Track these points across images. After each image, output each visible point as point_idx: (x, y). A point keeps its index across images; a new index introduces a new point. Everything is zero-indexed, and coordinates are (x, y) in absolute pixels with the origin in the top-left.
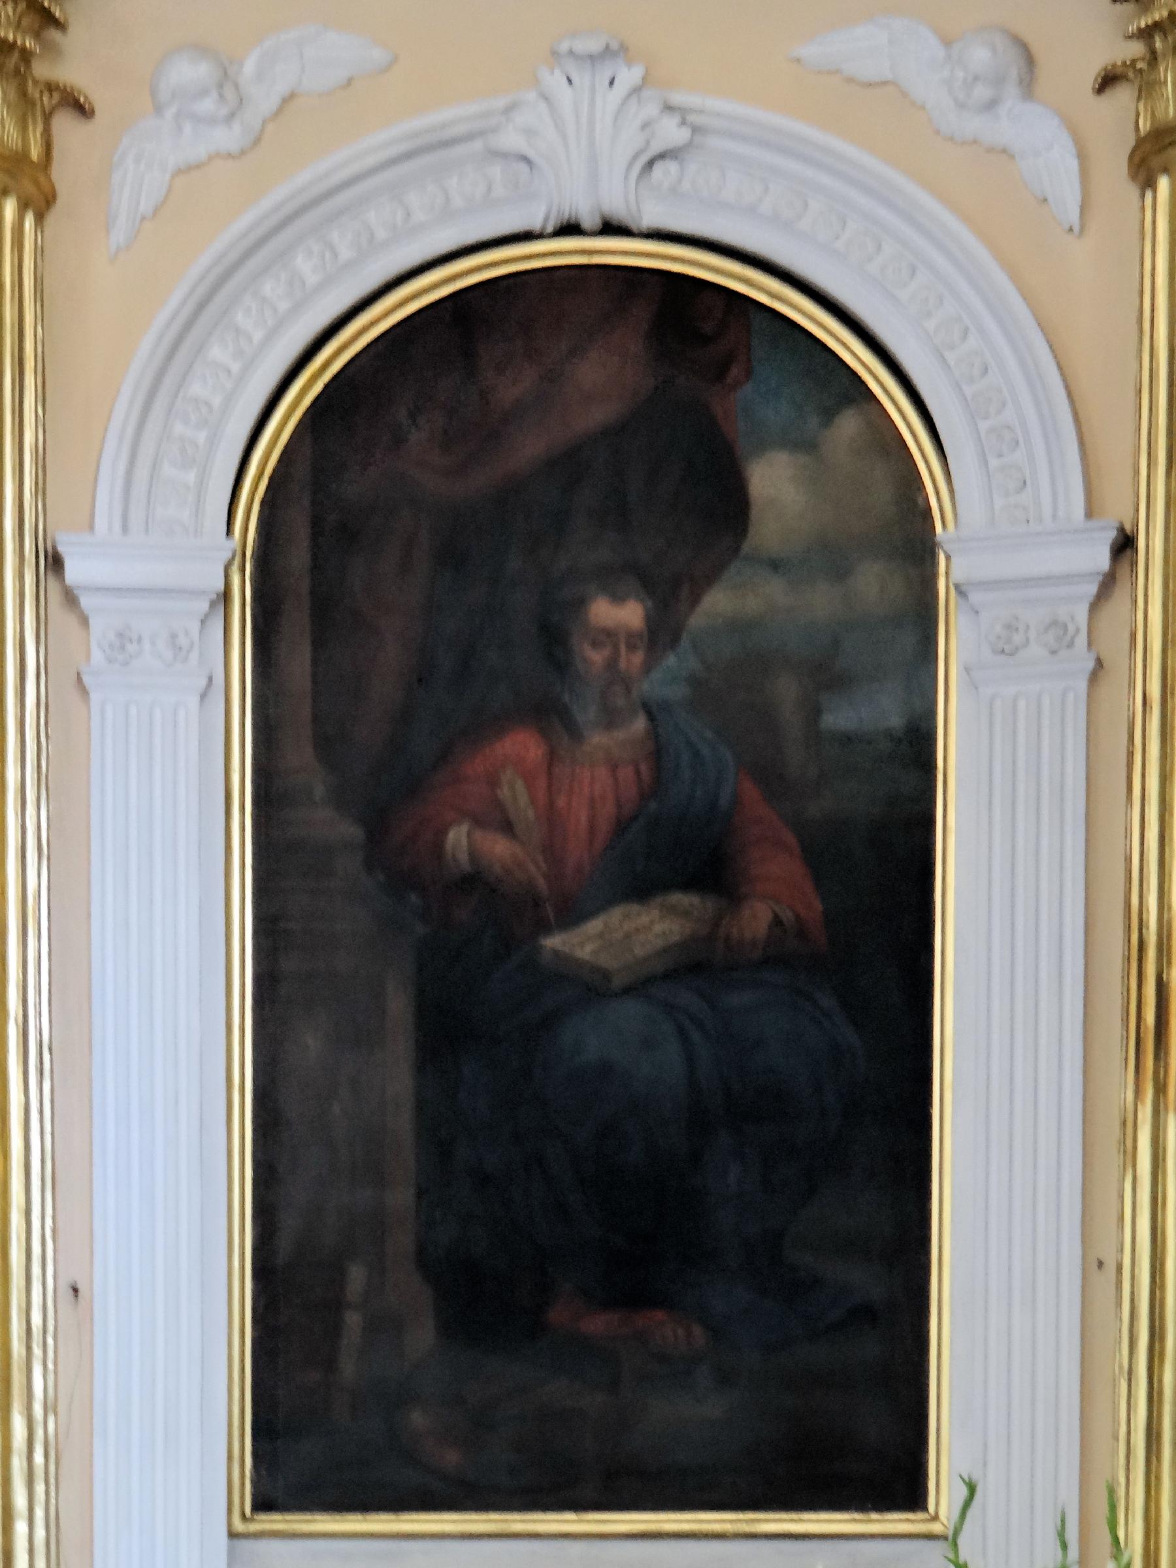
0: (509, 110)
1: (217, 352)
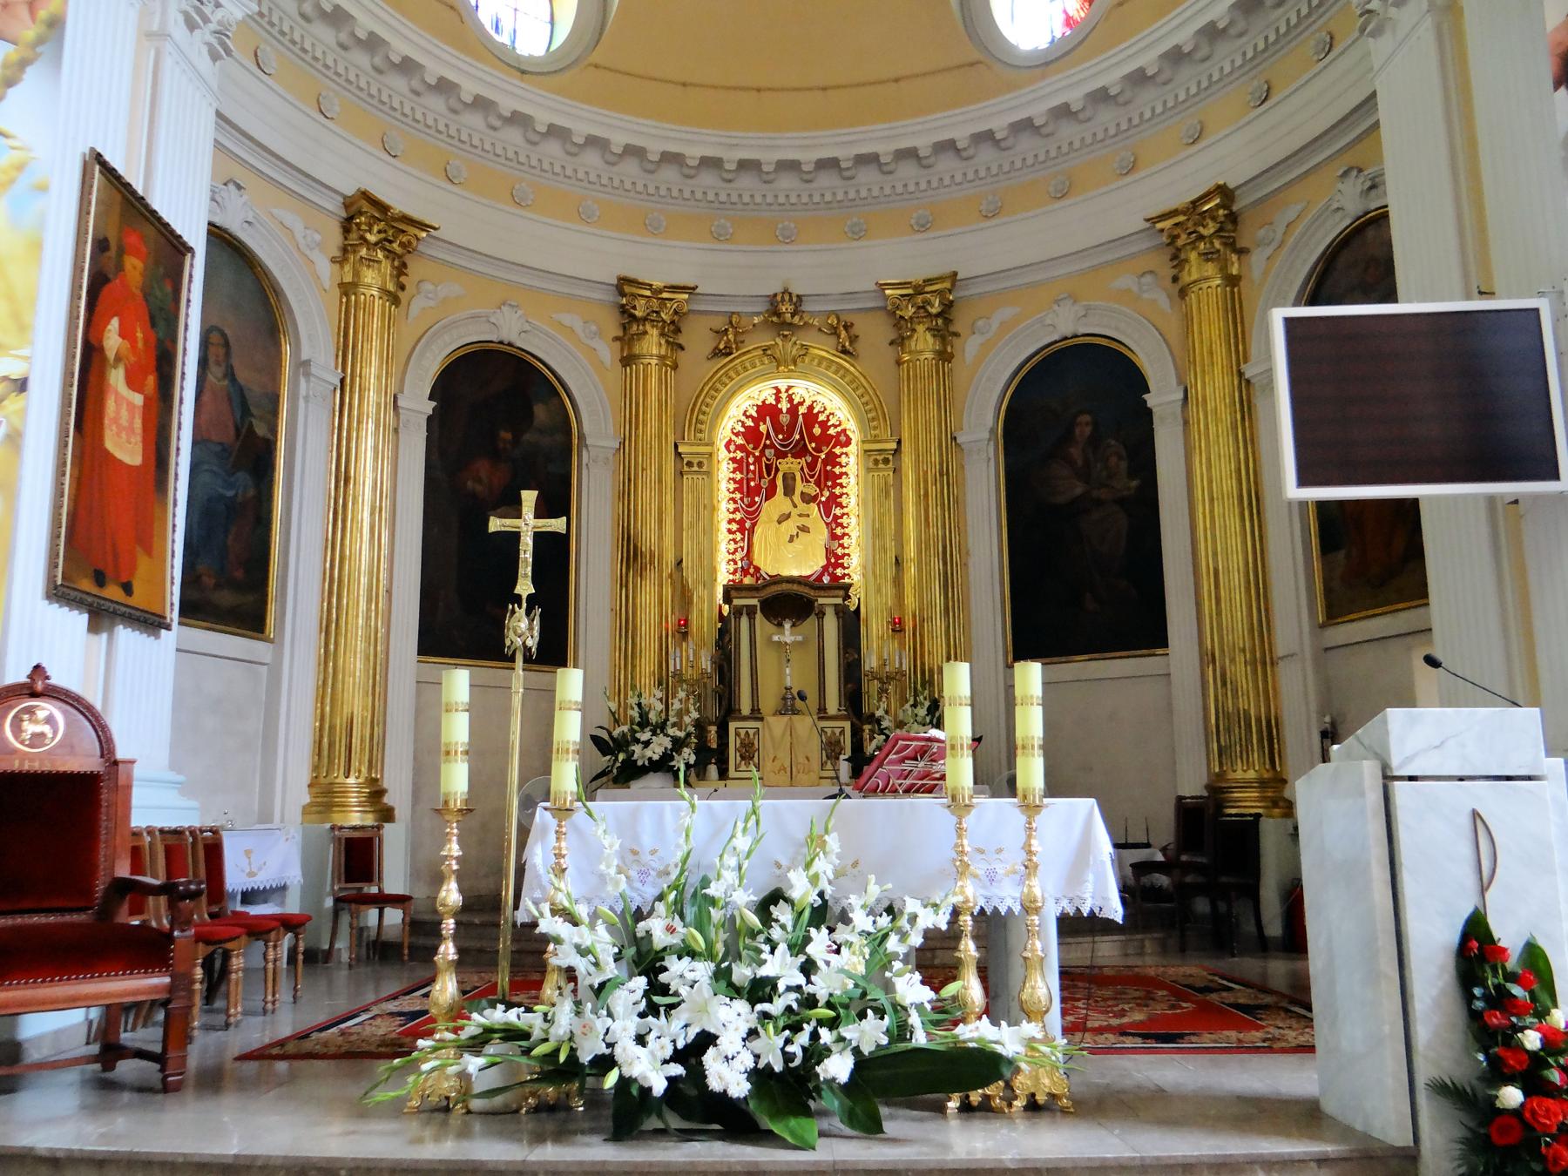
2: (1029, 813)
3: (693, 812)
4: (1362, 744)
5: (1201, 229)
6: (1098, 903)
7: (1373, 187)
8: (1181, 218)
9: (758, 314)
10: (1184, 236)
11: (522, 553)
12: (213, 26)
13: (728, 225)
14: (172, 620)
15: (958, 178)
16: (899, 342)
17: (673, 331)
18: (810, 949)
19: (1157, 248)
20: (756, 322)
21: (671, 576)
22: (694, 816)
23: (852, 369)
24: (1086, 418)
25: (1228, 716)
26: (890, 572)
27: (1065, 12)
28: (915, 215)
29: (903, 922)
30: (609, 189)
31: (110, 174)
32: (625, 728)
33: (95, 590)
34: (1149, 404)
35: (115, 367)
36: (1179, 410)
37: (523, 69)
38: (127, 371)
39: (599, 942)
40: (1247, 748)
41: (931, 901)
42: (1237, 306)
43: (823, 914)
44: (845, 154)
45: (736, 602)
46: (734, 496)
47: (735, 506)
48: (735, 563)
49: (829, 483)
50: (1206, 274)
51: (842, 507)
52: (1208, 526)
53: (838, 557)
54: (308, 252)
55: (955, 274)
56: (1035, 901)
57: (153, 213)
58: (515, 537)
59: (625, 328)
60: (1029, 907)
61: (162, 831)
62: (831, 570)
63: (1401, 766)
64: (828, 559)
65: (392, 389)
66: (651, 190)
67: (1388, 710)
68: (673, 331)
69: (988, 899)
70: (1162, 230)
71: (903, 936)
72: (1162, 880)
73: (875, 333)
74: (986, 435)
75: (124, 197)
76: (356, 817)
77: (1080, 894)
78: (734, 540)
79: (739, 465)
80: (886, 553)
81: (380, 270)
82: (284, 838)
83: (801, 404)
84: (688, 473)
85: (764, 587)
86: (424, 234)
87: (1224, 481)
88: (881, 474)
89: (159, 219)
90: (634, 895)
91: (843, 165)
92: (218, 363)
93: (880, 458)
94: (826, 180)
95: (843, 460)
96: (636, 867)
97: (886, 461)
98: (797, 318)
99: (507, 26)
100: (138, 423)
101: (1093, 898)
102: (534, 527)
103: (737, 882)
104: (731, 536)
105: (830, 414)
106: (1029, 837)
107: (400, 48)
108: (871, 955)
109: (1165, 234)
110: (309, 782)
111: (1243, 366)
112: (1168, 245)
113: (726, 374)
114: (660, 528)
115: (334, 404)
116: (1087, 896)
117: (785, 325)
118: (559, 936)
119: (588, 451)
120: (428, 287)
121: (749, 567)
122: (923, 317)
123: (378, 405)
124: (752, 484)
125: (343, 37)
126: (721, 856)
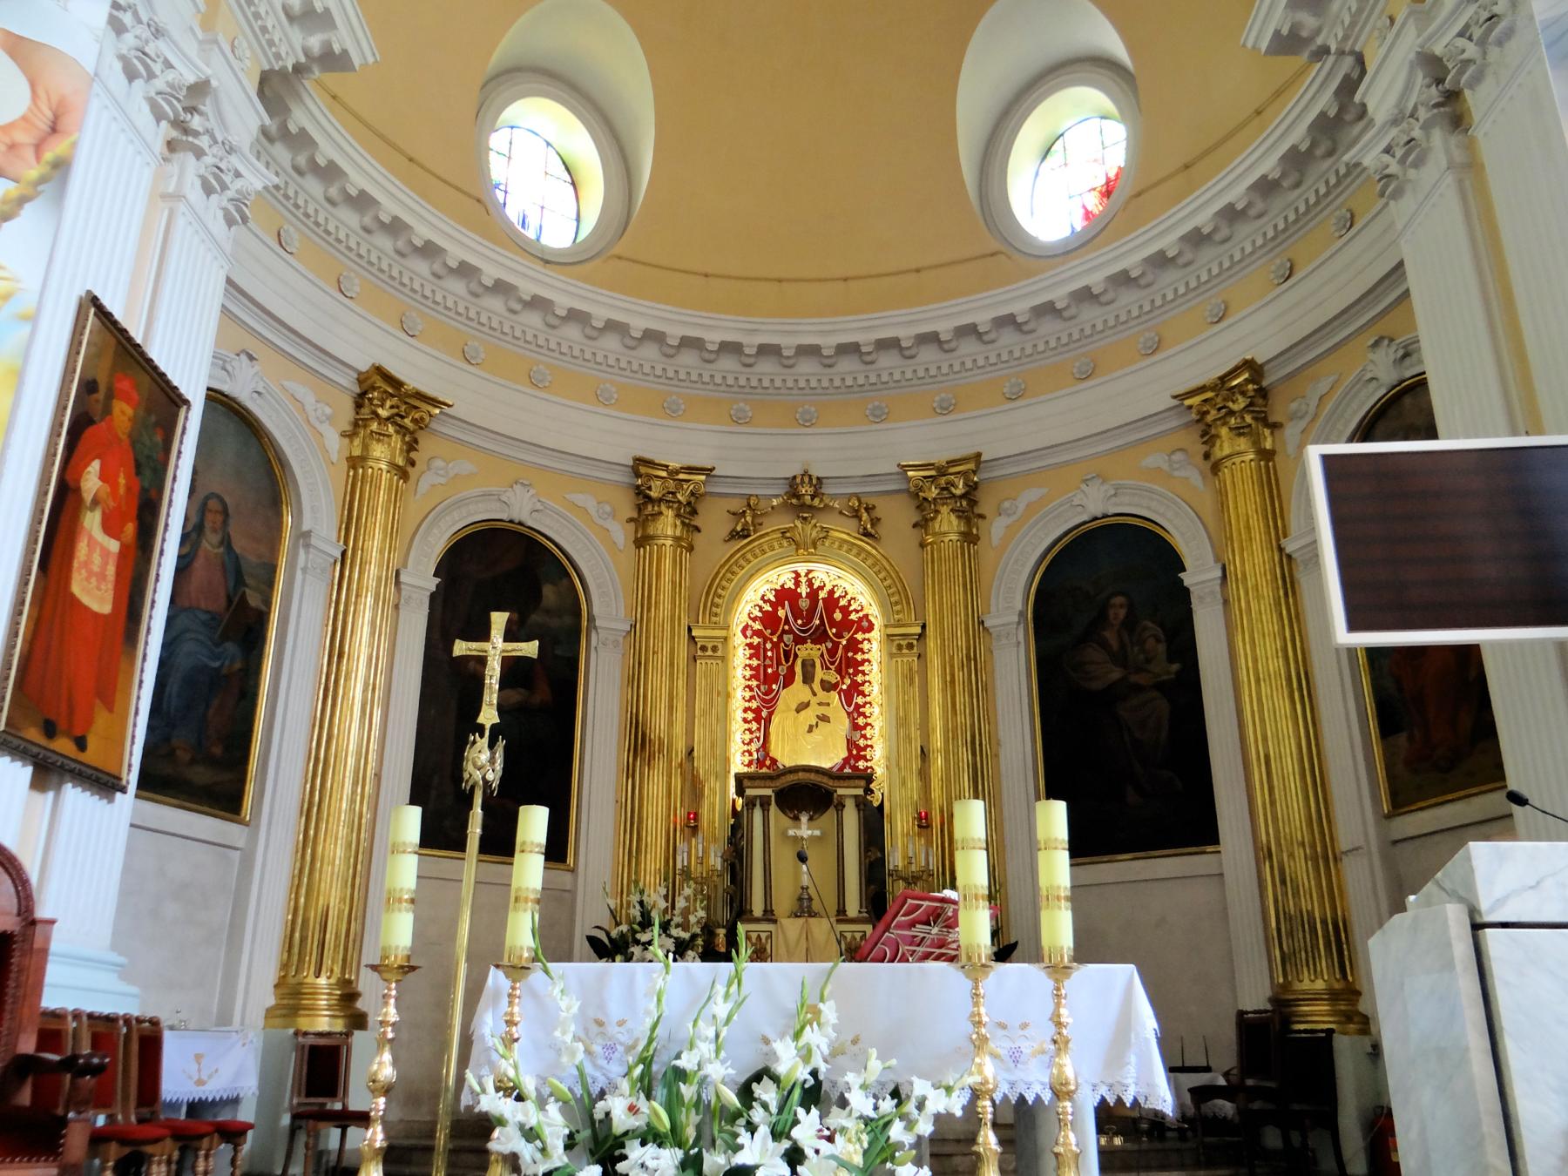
0: (505, 492)
1: (435, 531)
2: (1057, 976)
3: (667, 973)
4: (1444, 889)
5: (1230, 404)
6: (1144, 1090)
7: (1406, 355)
8: (1210, 395)
9: (776, 496)
10: (1213, 412)
11: (488, 678)
12: (230, 194)
13: (748, 408)
14: (128, 782)
15: (981, 362)
16: (922, 524)
17: (689, 513)
18: (795, 1133)
19: (1187, 425)
20: (775, 503)
21: (681, 765)
22: (669, 977)
23: (874, 552)
24: (1119, 600)
25: (1288, 918)
26: (916, 765)
27: (1084, 207)
28: (937, 398)
29: (910, 1107)
30: (627, 373)
31: (123, 335)
32: (624, 928)
33: (42, 741)
34: (1186, 583)
35: (92, 509)
36: (1218, 589)
37: (548, 259)
38: (104, 515)
39: (549, 1125)
40: (1313, 954)
41: (943, 1084)
42: (1273, 482)
43: (813, 1095)
44: (865, 338)
45: (749, 792)
46: (750, 683)
48: (751, 754)
49: (851, 671)
50: (1238, 448)
51: (865, 696)
52: (1255, 708)
53: (860, 749)
54: (317, 425)
55: (979, 455)
56: (1067, 1084)
57: (150, 361)
58: (482, 661)
59: (640, 509)
60: (1060, 1091)
61: (91, 1016)
62: (852, 762)
63: (1492, 910)
64: (849, 751)
65: (395, 563)
66: (671, 374)
67: (1470, 843)
68: (689, 513)
69: (1012, 1085)
70: (1190, 407)
71: (910, 1124)
72: (1226, 1107)
73: (897, 517)
74: (1016, 619)
75: (119, 342)
76: (324, 1022)
77: (1119, 1078)
78: (749, 730)
79: (756, 651)
80: (910, 743)
81: (389, 444)
82: (241, 1043)
83: (821, 588)
84: (701, 657)
85: (778, 776)
86: (437, 411)
87: (1270, 661)
89: (155, 368)
90: (598, 1074)
91: (864, 349)
92: (214, 531)
93: (904, 643)
94: (847, 365)
95: (866, 646)
96: (599, 1040)
97: (910, 646)
98: (816, 501)
99: (533, 222)
100: (111, 570)
101: (1136, 1084)
102: (504, 651)
103: (713, 1055)
104: (747, 726)
106: (1058, 1005)
107: (423, 232)
108: (870, 1144)
109: (1194, 410)
110: (276, 982)
111: (1282, 541)
112: (1198, 421)
113: (743, 556)
114: (671, 713)
115: (334, 577)
116: (1130, 1081)
117: (803, 507)
118: (502, 1115)
119: (598, 634)
120: (439, 463)
121: (764, 757)
122: (946, 498)
123: (379, 579)
124: (770, 671)
125: (367, 220)
126: (695, 1021)
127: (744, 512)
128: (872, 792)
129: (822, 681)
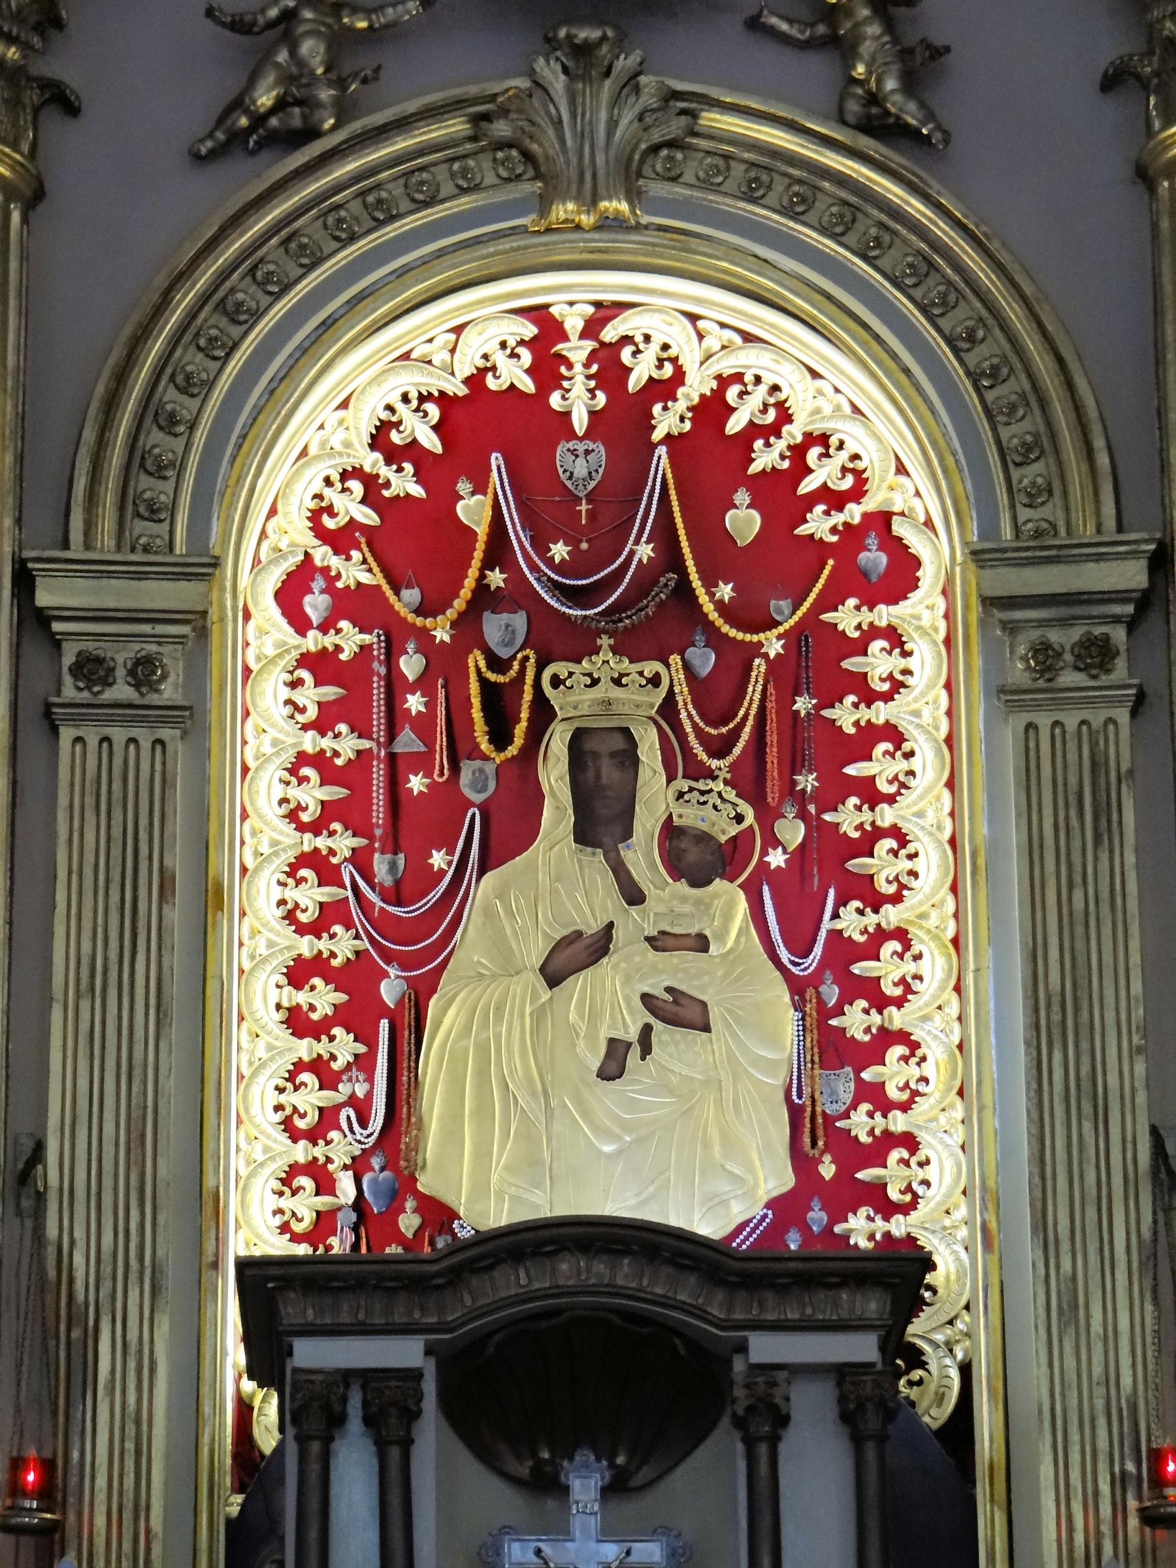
23: (916, 207)
46: (322, 842)
47: (327, 893)
48: (325, 1185)
49: (807, 781)
62: (817, 1216)
64: (802, 1163)
78: (319, 1067)
80: (1101, 1119)
84: (82, 713)
88: (1071, 720)
93: (1065, 638)
104: (305, 1049)
105: (811, 439)
124: (416, 783)
127: (289, 16)
128: (916, 1358)
129: (670, 830)
